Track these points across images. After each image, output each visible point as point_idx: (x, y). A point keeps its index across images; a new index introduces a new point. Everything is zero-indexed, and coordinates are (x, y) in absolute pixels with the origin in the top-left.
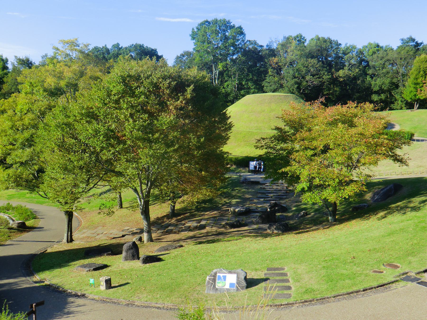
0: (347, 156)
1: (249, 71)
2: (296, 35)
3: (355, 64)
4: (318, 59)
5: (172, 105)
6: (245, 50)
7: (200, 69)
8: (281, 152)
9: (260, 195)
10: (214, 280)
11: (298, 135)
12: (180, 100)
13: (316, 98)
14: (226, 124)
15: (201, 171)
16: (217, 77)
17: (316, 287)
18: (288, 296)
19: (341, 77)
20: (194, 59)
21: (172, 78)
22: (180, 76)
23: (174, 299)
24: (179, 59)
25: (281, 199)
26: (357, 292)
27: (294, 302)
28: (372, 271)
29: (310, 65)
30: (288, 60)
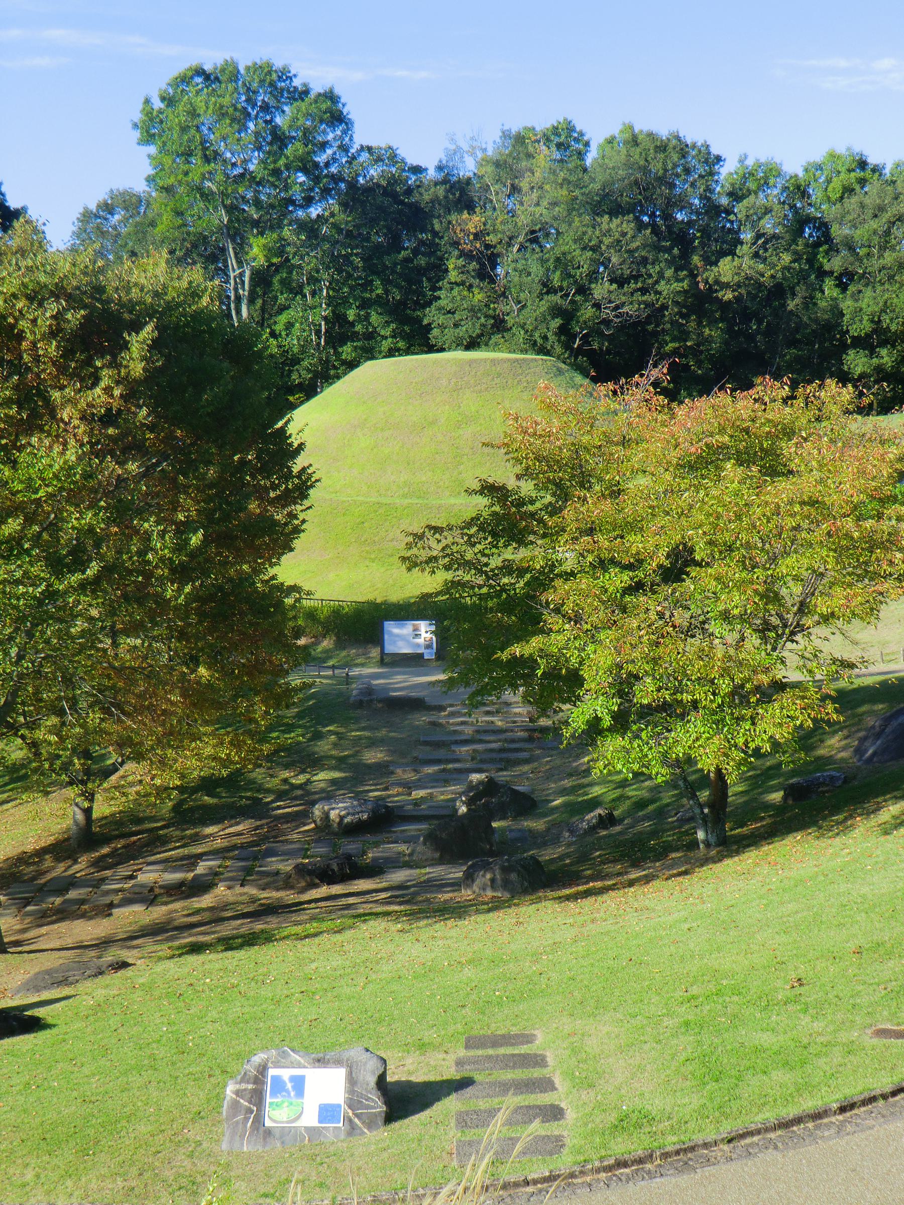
0: (761, 589)
1: (372, 268)
2: (548, 125)
3: (775, 237)
4: (637, 219)
5: (72, 404)
6: (352, 185)
7: (179, 260)
8: (505, 580)
9: (422, 752)
10: (257, 1097)
11: (569, 513)
12: (102, 384)
13: (635, 366)
14: (289, 476)
15: (193, 661)
16: (244, 293)
17: (656, 1104)
18: (550, 1147)
19: (726, 286)
20: (153, 224)
21: (69, 297)
22: (99, 289)
23: (94, 1185)
24: (93, 222)
25: (509, 764)
26: (817, 1116)
27: (577, 1169)
28: (869, 1031)
29: (607, 241)
30: (523, 220)
